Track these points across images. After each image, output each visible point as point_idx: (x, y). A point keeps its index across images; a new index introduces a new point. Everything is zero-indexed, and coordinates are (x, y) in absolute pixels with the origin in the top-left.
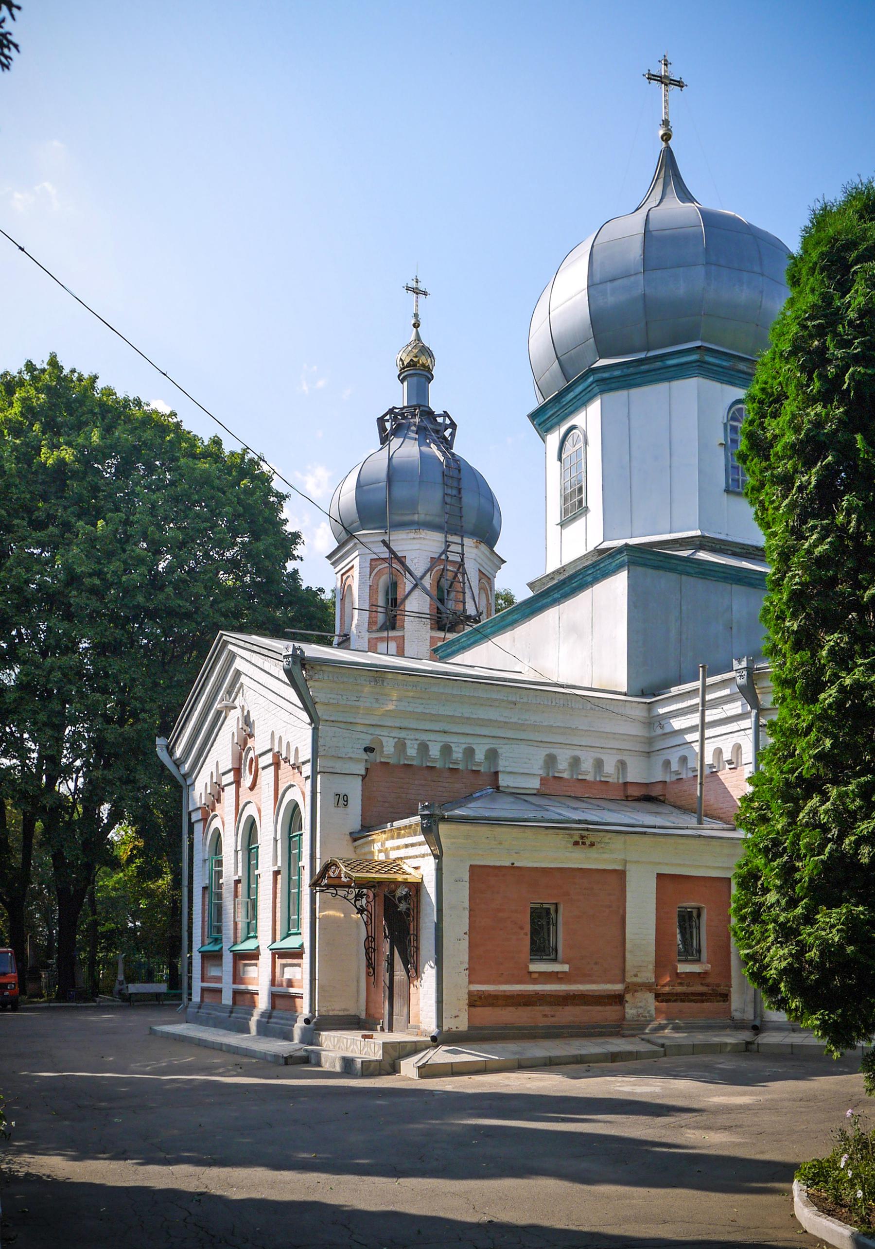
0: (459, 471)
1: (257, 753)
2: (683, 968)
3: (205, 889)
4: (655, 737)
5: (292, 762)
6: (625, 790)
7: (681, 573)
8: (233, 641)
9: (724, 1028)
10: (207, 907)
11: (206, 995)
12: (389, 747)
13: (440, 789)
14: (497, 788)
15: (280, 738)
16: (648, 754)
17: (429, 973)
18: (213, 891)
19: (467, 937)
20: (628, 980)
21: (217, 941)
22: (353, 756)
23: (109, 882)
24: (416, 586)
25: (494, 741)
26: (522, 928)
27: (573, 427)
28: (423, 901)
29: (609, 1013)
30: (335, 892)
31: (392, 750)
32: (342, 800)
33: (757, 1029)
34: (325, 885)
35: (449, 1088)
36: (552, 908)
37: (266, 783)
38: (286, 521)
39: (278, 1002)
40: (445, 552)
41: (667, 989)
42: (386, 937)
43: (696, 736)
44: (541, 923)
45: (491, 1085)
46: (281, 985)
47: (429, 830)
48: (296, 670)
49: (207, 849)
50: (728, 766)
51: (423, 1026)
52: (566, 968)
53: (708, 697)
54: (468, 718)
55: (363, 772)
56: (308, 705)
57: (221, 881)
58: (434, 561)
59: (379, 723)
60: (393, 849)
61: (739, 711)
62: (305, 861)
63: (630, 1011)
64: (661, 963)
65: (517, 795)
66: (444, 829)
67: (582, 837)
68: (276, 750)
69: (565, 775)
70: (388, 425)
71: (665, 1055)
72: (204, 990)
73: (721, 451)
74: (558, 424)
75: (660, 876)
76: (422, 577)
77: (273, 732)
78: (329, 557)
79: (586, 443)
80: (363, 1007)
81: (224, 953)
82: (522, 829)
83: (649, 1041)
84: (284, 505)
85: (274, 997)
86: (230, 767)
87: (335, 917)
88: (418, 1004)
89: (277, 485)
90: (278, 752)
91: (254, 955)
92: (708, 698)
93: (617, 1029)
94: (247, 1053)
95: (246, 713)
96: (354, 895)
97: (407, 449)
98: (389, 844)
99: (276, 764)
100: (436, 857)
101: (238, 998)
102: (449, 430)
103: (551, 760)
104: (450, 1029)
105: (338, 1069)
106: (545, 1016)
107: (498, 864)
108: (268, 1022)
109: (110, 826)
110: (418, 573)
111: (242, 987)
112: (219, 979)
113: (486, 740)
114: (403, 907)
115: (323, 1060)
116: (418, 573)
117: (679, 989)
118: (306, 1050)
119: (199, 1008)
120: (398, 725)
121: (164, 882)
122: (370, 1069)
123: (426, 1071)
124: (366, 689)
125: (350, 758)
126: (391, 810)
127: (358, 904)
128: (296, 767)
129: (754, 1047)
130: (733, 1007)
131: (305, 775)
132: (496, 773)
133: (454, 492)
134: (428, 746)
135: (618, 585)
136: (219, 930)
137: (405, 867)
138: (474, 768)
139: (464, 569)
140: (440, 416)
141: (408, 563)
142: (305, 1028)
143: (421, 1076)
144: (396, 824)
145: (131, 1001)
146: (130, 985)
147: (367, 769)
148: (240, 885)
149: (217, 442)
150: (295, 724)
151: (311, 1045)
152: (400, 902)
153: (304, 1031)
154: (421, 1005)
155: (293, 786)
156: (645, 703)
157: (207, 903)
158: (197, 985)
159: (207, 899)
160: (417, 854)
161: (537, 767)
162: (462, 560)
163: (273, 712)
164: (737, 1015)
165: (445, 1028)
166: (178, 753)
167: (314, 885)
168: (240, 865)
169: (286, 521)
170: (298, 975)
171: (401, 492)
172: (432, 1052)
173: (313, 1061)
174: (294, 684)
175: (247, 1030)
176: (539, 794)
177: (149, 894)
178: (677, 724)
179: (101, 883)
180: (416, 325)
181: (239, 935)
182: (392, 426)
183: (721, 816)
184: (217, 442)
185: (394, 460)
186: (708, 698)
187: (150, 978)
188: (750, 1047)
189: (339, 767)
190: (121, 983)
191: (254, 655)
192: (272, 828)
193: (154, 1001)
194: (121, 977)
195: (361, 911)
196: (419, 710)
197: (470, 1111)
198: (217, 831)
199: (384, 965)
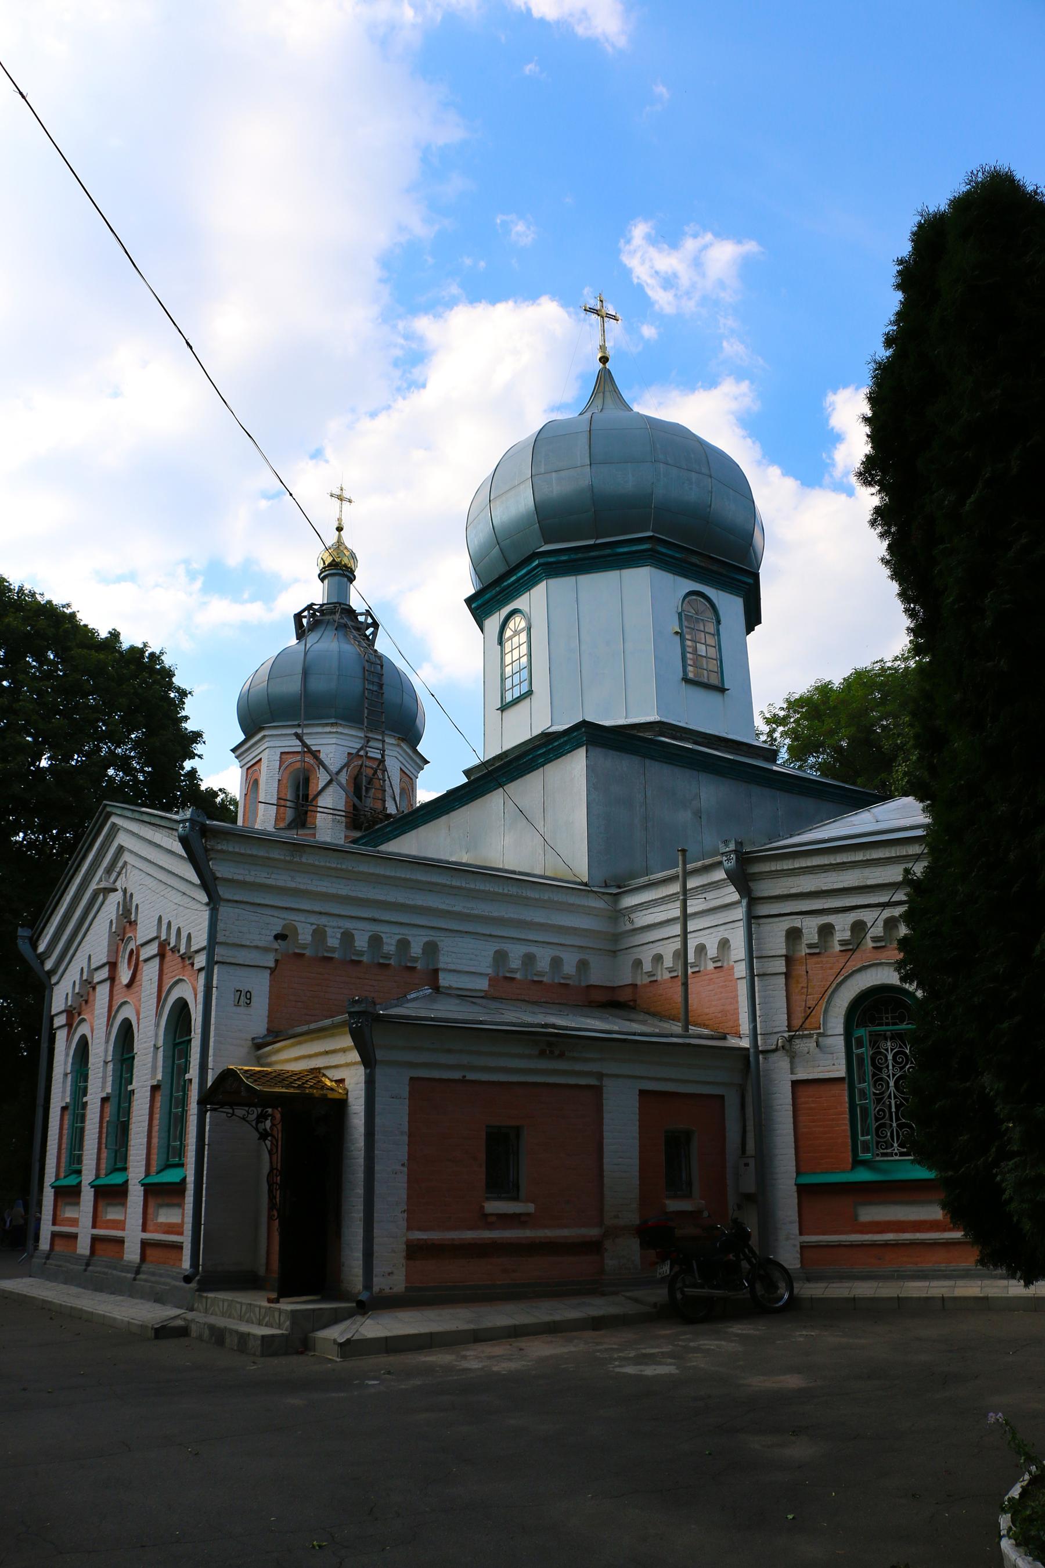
0: (382, 666)
5: (183, 951)
8: (119, 812)
11: (57, 1241)
12: (305, 935)
14: (437, 989)
15: (169, 923)
24: (330, 782)
30: (230, 1111)
31: (310, 938)
32: (244, 998)
37: (148, 978)
38: (186, 718)
39: (58, 1241)
43: (677, 929)
55: (272, 964)
56: (208, 883)
62: (193, 1073)
63: (610, 1263)
65: (464, 996)
68: (163, 937)
72: (54, 1235)
76: (338, 773)
77: (160, 917)
78: (233, 750)
81: (130, 1187)
84: (185, 701)
86: (105, 960)
90: (165, 940)
96: (255, 1116)
97: (327, 644)
99: (161, 955)
101: (99, 1246)
102: (371, 630)
104: (381, 1290)
116: (334, 769)
119: (48, 1257)
127: (261, 1126)
131: (197, 966)
132: (436, 971)
133: (375, 688)
134: (353, 935)
138: (409, 964)
139: (384, 766)
140: (361, 614)
141: (322, 756)
147: (277, 961)
149: (115, 635)
150: (188, 905)
156: (611, 894)
158: (47, 1229)
161: (485, 966)
162: (383, 756)
165: (376, 1289)
166: (41, 949)
169: (186, 718)
170: (179, 1217)
174: (193, 858)
176: (486, 996)
178: (643, 919)
180: (339, 529)
182: (309, 622)
183: (707, 1022)
184: (115, 635)
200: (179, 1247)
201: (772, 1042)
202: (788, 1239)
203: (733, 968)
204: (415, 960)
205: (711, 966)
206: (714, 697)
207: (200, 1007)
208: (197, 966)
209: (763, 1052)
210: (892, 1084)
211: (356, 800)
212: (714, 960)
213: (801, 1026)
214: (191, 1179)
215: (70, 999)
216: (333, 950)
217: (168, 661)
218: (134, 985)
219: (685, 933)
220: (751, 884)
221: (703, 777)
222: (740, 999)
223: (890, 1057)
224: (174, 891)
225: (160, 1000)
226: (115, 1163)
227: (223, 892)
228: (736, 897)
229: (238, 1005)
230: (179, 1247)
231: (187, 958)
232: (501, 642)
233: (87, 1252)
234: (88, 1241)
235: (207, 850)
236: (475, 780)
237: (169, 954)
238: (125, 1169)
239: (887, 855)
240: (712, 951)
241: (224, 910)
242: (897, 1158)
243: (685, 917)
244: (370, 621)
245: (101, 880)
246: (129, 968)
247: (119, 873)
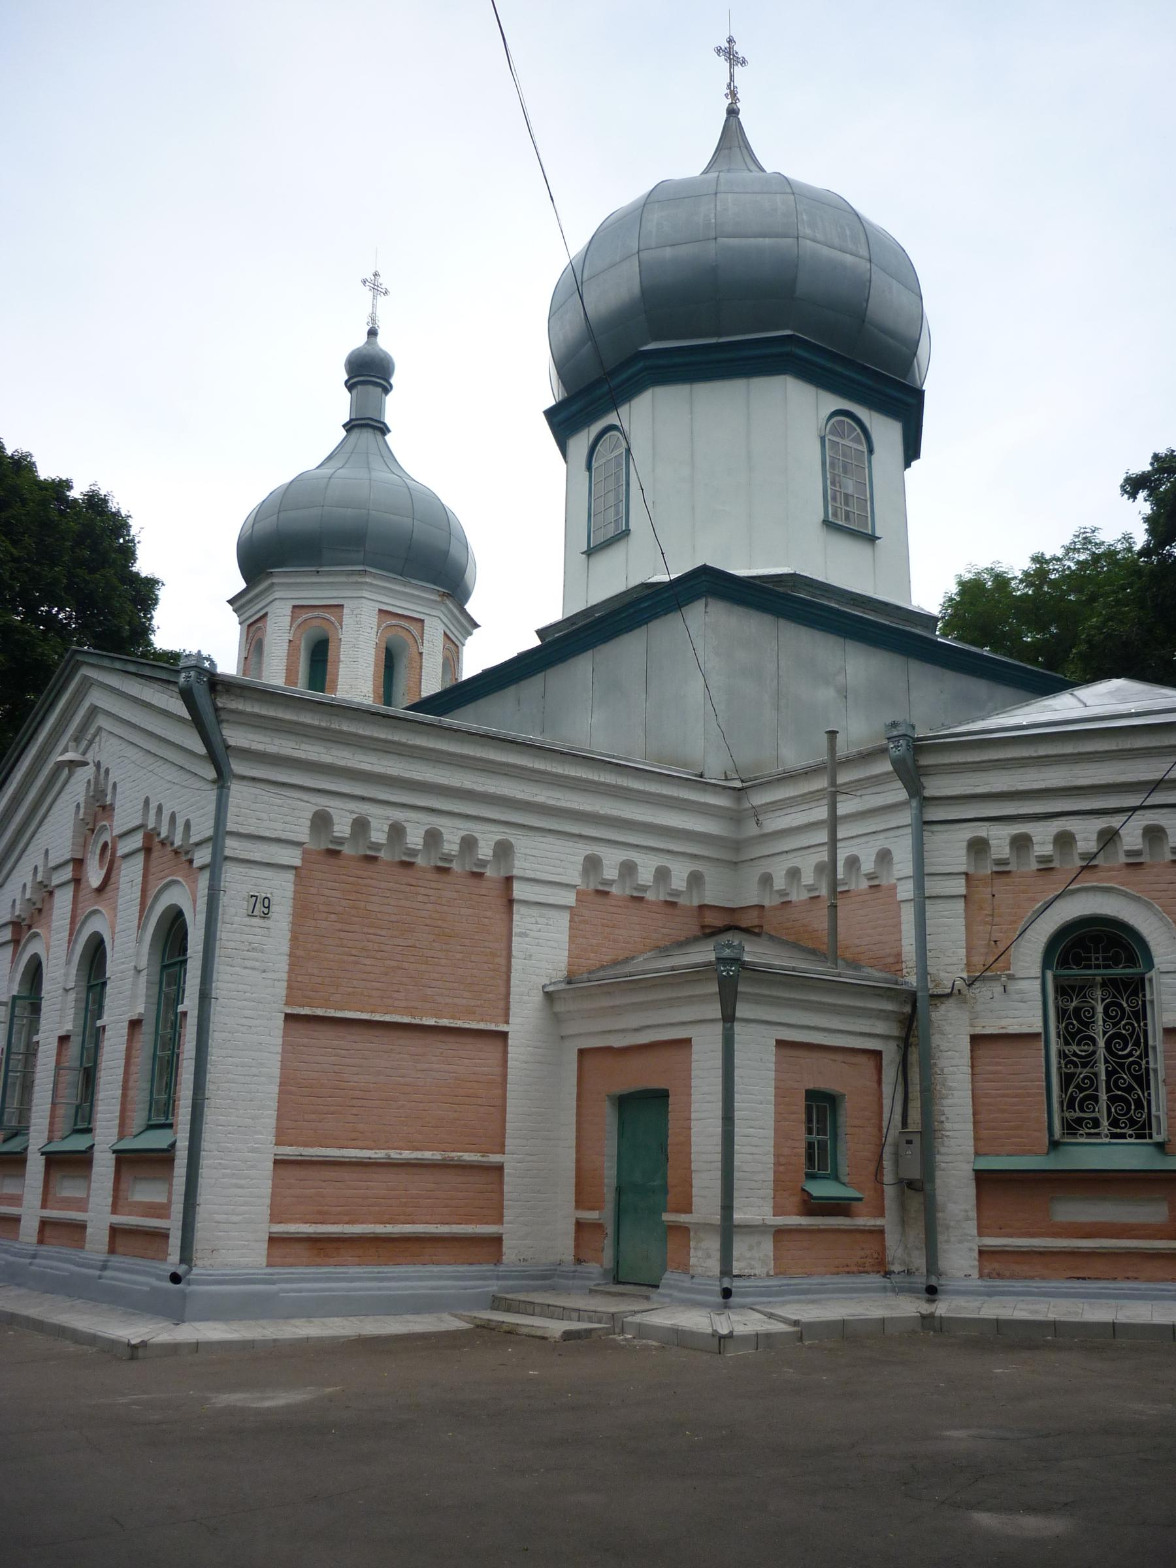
1: (116, 832)
13: (421, 898)
15: (160, 808)
32: (262, 907)
33: (932, 1291)
43: (823, 836)
68: (151, 825)
78: (230, 602)
86: (68, 856)
92: (840, 781)
99: (147, 850)
108: (100, 1277)
126: (339, 926)
132: (509, 880)
156: (734, 788)
163: (150, 768)
200: (163, 1235)
203: (895, 887)
205: (864, 884)
207: (202, 918)
208: (196, 864)
212: (870, 877)
213: (989, 969)
214: (183, 1144)
215: (18, 906)
218: (109, 888)
219: (833, 841)
220: (923, 779)
222: (904, 927)
224: (167, 766)
226: (75, 1124)
227: (238, 767)
228: (903, 795)
229: (251, 915)
230: (163, 1235)
231: (183, 855)
232: (589, 467)
234: (36, 1225)
235: (217, 710)
236: (549, 643)
237: (157, 847)
238: (88, 1131)
240: (868, 865)
241: (236, 790)
242: (1107, 1140)
243: (833, 822)
246: (101, 867)
247: (91, 742)
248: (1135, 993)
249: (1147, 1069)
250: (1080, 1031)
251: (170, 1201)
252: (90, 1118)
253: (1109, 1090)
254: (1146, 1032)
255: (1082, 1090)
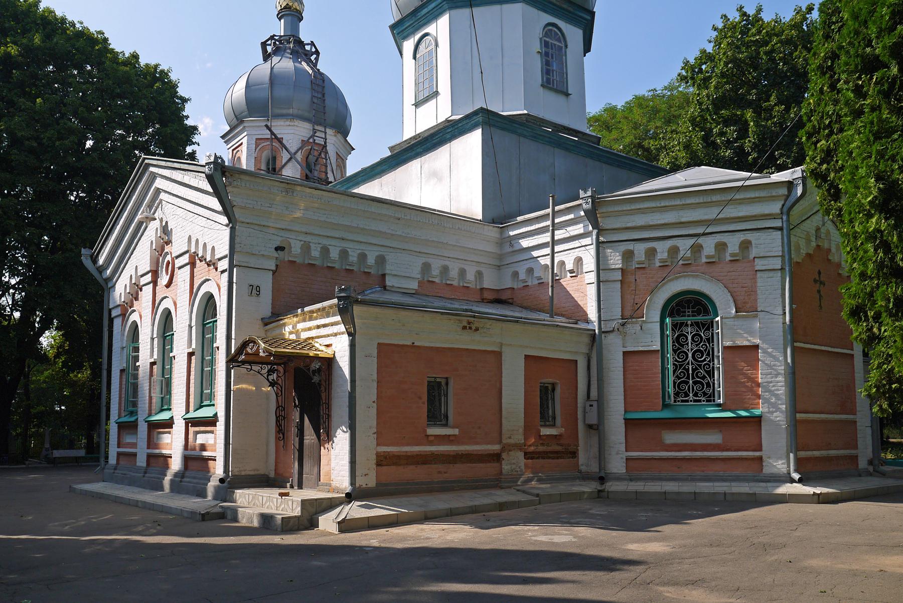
2: (546, 431)
3: (122, 371)
4: (508, 253)
6: (482, 294)
7: (520, 135)
9: (574, 479)
10: (124, 386)
14: (384, 287)
16: (499, 267)
17: (342, 439)
18: (130, 372)
19: (375, 405)
20: (504, 441)
21: (132, 413)
22: (266, 253)
23: (41, 376)
24: (290, 159)
25: (382, 249)
26: (420, 398)
27: (427, 34)
28: (335, 374)
29: (486, 470)
31: (299, 251)
33: (602, 480)
34: (241, 362)
35: (375, 543)
36: (443, 382)
38: (187, 117)
39: (121, 458)
40: (312, 136)
41: (532, 449)
42: (296, 406)
43: (548, 251)
44: (436, 392)
45: (414, 538)
46: (194, 449)
47: (345, 311)
48: (218, 175)
49: (125, 338)
50: (569, 275)
51: (334, 484)
52: (456, 431)
53: (557, 221)
54: (363, 229)
55: (274, 268)
56: (227, 211)
57: (137, 364)
58: (304, 143)
59: (289, 228)
60: (305, 330)
61: (582, 231)
63: (506, 467)
64: (528, 428)
66: (357, 310)
67: (469, 323)
68: (193, 250)
69: (437, 280)
70: (269, 49)
71: (540, 503)
72: (119, 454)
73: (538, 57)
74: (413, 33)
75: (527, 357)
78: (223, 137)
79: (437, 45)
80: (273, 468)
82: (421, 314)
83: (524, 492)
85: (187, 460)
86: (149, 269)
87: (247, 390)
88: (329, 464)
89: (182, 91)
90: (195, 253)
91: (169, 424)
93: (497, 482)
94: (163, 510)
95: (164, 224)
97: (285, 64)
98: (300, 326)
99: (192, 264)
100: (350, 334)
101: (152, 460)
102: (315, 56)
103: (426, 267)
105: (256, 523)
106: (439, 472)
107: (401, 343)
109: (41, 333)
110: (293, 150)
111: (157, 451)
112: (134, 445)
113: (376, 248)
114: (316, 379)
115: (240, 516)
116: (293, 150)
117: (541, 448)
118: (222, 507)
119: (115, 469)
120: (304, 230)
121: (84, 375)
122: (290, 525)
123: (346, 526)
124: (278, 198)
125: (263, 255)
127: (271, 378)
128: (212, 264)
129: (605, 494)
130: (580, 463)
131: (220, 269)
132: (384, 275)
133: (320, 96)
135: (475, 138)
136: (135, 404)
137: (317, 345)
140: (308, 44)
142: (218, 486)
143: (342, 531)
144: (307, 309)
145: (56, 464)
146: (55, 452)
147: (277, 266)
148: (155, 367)
151: (225, 502)
152: (314, 375)
153: (217, 490)
154: (333, 465)
155: (208, 280)
157: (124, 383)
159: (124, 380)
160: (329, 333)
161: (416, 272)
162: (325, 143)
164: (583, 468)
165: (357, 485)
166: (101, 261)
167: (232, 361)
168: (156, 350)
169: (187, 117)
170: (214, 442)
171: (280, 92)
172: (347, 508)
173: (229, 517)
174: (217, 193)
175: (161, 488)
177: (73, 384)
178: (525, 243)
179: (34, 378)
181: (153, 408)
182: (273, 48)
184: (135, 56)
185: (274, 70)
186: (557, 221)
187: (71, 446)
188: (602, 494)
189: (253, 262)
190: (47, 450)
191: (174, 172)
192: (187, 317)
193: (74, 464)
194: (47, 445)
195: (272, 384)
196: (322, 219)
197: (421, 572)
198: (135, 324)
199: (294, 430)
201: (614, 324)
202: (617, 454)
204: (370, 267)
206: (561, 99)
208: (220, 269)
209: (604, 332)
210: (690, 355)
211: (308, 173)
213: (632, 314)
216: (315, 259)
217: (173, 77)
221: (557, 150)
223: (690, 338)
225: (193, 293)
232: (415, 58)
233: (144, 465)
239: (697, 201)
244: (314, 50)
245: (143, 212)
246: (167, 273)
248: (708, 329)
249: (713, 368)
250: (679, 349)
251: (215, 443)
252: (169, 403)
253: (693, 378)
254: (713, 349)
255: (679, 378)
